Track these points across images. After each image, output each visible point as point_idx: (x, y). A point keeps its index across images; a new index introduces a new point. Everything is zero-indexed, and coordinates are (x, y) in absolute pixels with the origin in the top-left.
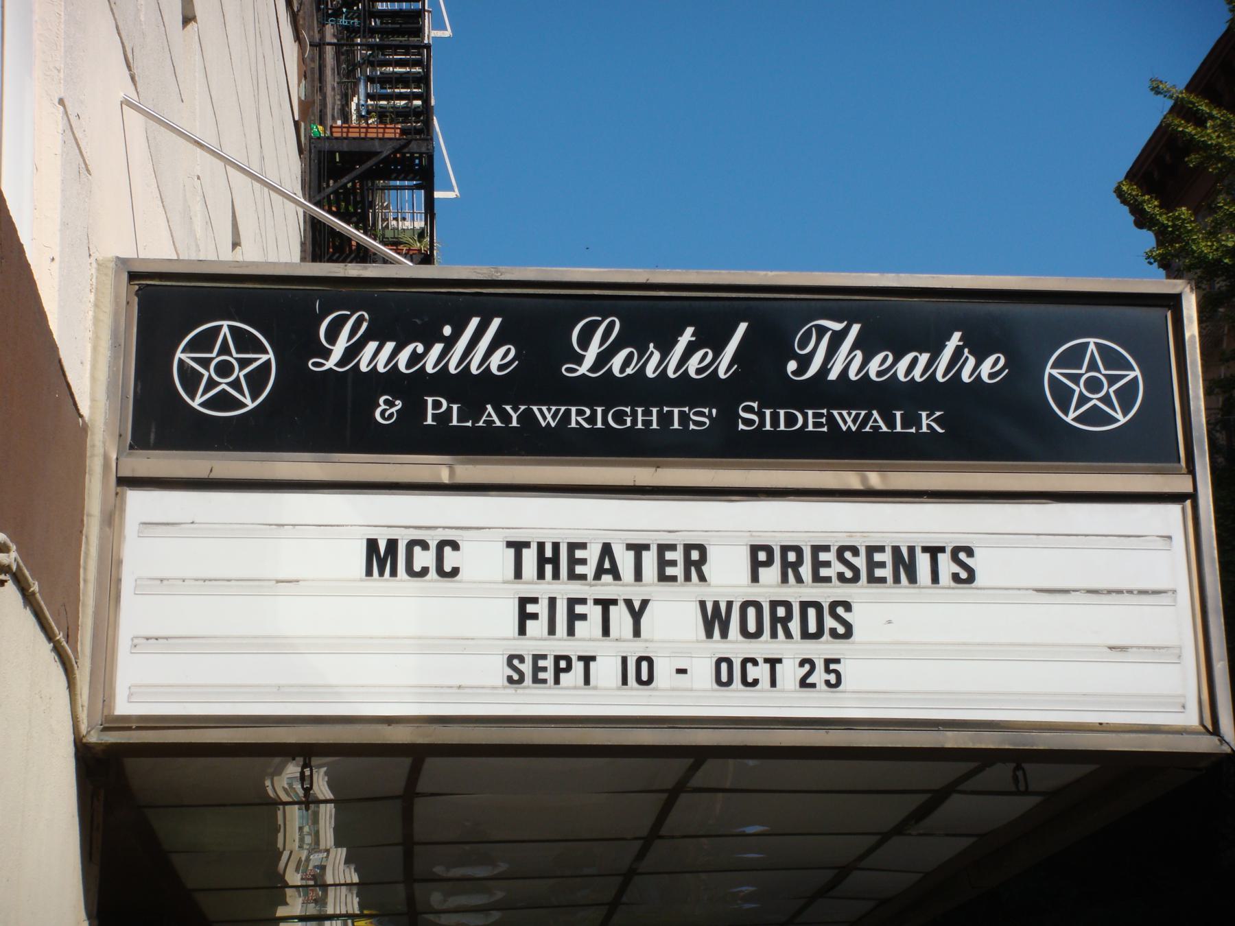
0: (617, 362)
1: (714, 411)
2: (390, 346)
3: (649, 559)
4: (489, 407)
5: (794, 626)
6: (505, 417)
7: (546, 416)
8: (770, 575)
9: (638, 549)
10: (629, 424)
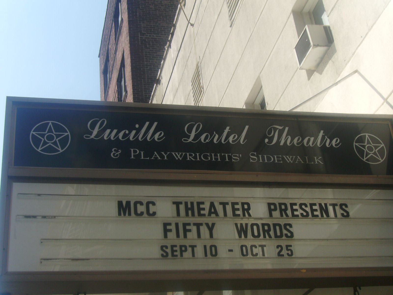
0: (203, 137)
1: (241, 155)
2: (115, 131)
3: (229, 208)
4: (155, 152)
5: (272, 233)
6: (162, 156)
7: (178, 156)
8: (276, 214)
9: (224, 204)
10: (209, 159)
